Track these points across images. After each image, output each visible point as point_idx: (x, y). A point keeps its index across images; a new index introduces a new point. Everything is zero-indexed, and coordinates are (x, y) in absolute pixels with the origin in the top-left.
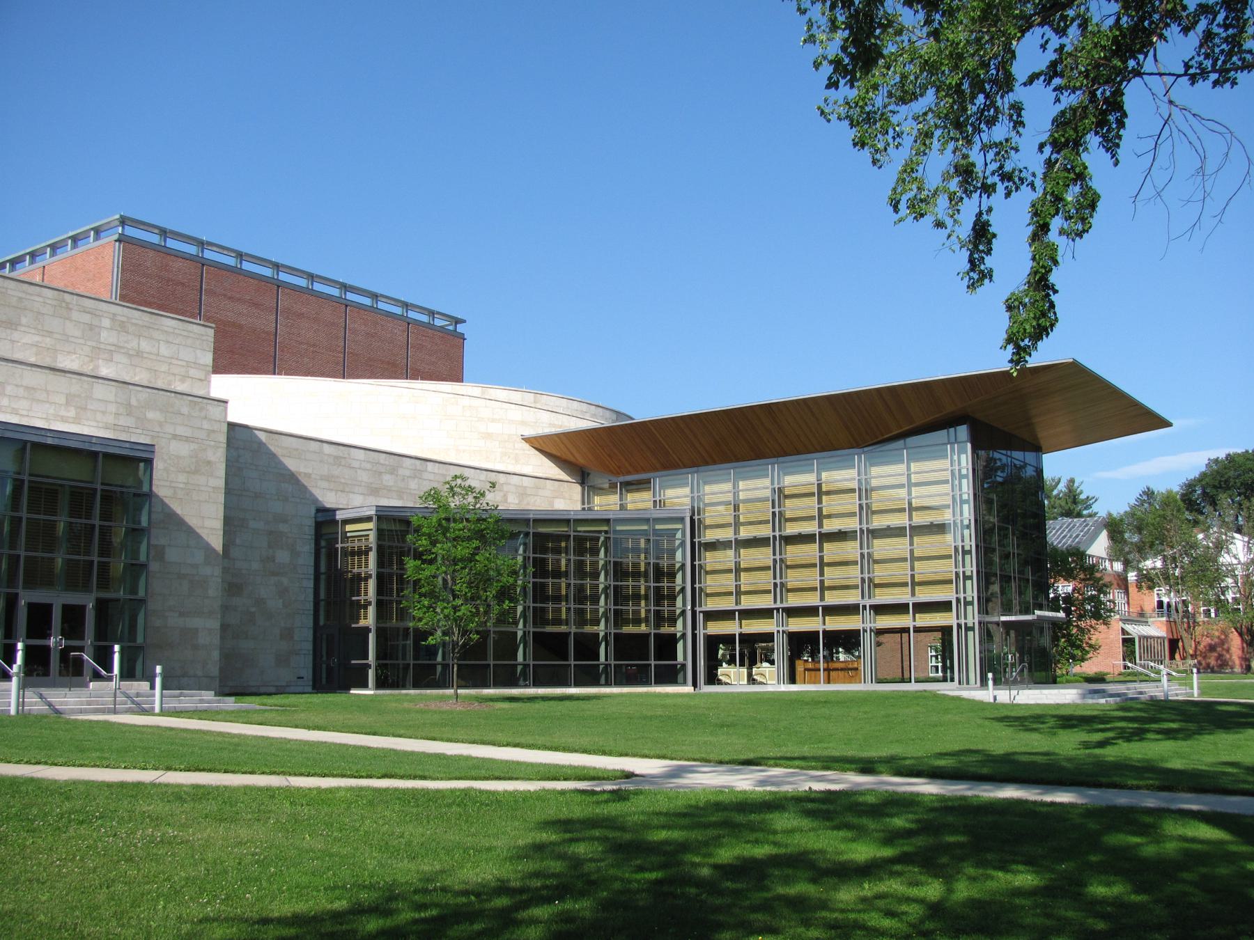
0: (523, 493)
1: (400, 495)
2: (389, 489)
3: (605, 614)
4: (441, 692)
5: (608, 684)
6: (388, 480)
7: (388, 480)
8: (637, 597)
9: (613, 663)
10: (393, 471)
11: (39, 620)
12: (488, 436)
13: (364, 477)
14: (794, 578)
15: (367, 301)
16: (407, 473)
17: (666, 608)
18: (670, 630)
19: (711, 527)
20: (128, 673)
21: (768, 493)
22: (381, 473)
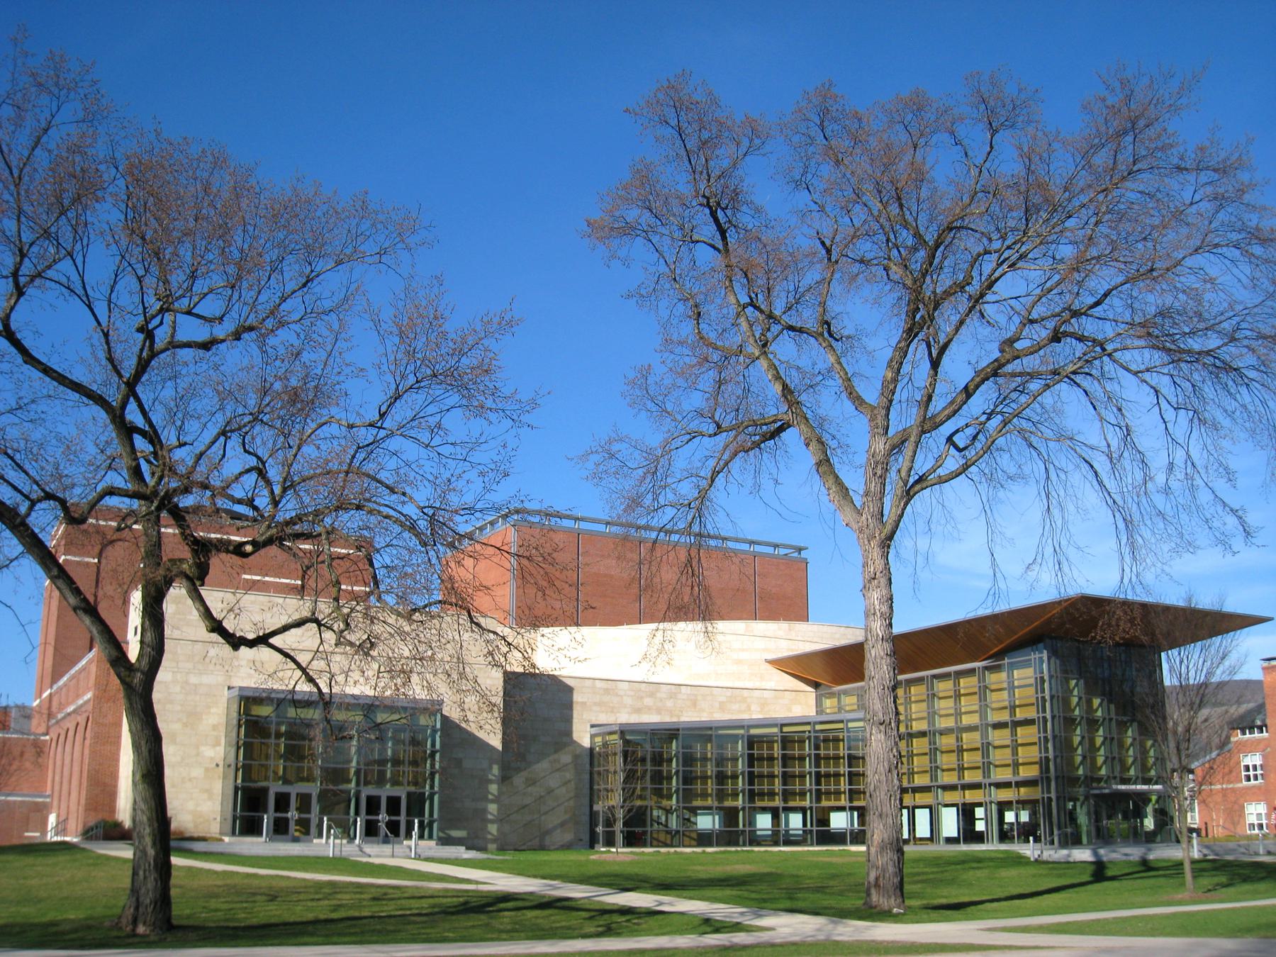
0: (763, 704)
1: (659, 711)
2: (649, 708)
3: (677, 791)
4: (836, 848)
5: (812, 845)
6: (648, 701)
7: (648, 701)
8: (705, 778)
9: (815, 828)
10: (652, 695)
11: (373, 805)
12: (739, 662)
13: (628, 701)
14: (977, 758)
15: (770, 550)
16: (664, 696)
17: (699, 786)
18: (734, 804)
19: (922, 718)
20: (421, 837)
21: (1032, 681)
22: (642, 698)
